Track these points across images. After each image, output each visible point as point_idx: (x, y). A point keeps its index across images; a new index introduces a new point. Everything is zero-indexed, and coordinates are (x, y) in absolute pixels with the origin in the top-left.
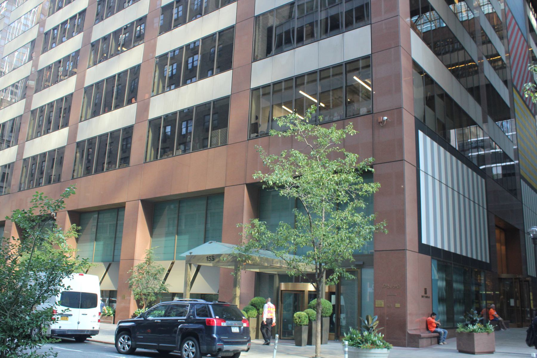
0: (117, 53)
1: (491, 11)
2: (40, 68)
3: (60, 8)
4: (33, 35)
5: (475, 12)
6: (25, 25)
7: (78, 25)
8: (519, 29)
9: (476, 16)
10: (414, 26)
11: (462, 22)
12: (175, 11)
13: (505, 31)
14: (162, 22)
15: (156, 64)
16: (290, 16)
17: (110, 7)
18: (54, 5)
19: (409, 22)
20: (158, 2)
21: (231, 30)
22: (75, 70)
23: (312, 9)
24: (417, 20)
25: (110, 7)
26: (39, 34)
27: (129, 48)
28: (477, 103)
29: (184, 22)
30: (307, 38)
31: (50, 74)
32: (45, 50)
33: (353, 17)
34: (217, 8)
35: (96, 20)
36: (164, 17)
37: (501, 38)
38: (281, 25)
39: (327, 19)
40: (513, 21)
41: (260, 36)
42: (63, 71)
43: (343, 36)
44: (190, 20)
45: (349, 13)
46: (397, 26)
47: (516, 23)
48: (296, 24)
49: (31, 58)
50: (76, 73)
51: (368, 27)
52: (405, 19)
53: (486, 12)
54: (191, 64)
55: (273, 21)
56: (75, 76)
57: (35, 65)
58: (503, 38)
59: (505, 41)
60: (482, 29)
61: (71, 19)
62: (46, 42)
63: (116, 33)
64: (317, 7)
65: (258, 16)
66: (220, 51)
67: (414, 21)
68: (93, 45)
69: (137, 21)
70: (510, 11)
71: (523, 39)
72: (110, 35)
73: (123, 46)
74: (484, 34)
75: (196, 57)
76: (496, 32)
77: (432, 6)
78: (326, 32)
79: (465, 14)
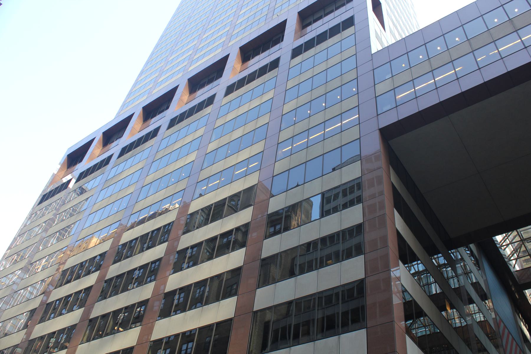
0: (113, 332)
1: (482, 319)
2: (32, 337)
3: (68, 282)
4: (35, 304)
5: (468, 319)
6: (31, 293)
7: (81, 300)
8: (513, 339)
9: (469, 322)
10: (408, 331)
11: (456, 328)
12: (177, 297)
13: (500, 339)
14: (162, 306)
15: (150, 347)
16: (288, 314)
17: (116, 286)
18: (64, 278)
19: (404, 325)
20: (162, 287)
21: (229, 322)
22: (68, 344)
23: (309, 307)
24: (411, 323)
25: (116, 286)
26: (42, 303)
27: (125, 329)
28: (294, 31)
29: (184, 310)
30: (303, 335)
31: (41, 344)
32: (42, 320)
33: (348, 320)
34: (218, 300)
35: (100, 296)
36: (165, 302)
37: (497, 347)
38: (277, 321)
39: (323, 318)
40: (506, 331)
41: (257, 330)
42: (54, 343)
43: (339, 338)
44: (190, 309)
45: (345, 314)
46: (392, 329)
47: (509, 333)
48: (293, 321)
49: (26, 326)
50: (66, 347)
51: (363, 332)
52: (401, 324)
53: (478, 320)
54: (184, 351)
55: (270, 316)
56: (66, 350)
57: (29, 334)
58: (498, 346)
59: (501, 350)
60: (476, 337)
61: (76, 293)
62: (46, 312)
63: (116, 313)
64: (314, 306)
65: (257, 312)
66: (215, 341)
67: (409, 325)
68: (91, 321)
69: (138, 303)
70: (501, 320)
71: (518, 349)
72: (109, 313)
73: (121, 325)
74: (479, 342)
75: (190, 345)
76: (490, 340)
77: (425, 313)
78: (322, 331)
79: (457, 321)
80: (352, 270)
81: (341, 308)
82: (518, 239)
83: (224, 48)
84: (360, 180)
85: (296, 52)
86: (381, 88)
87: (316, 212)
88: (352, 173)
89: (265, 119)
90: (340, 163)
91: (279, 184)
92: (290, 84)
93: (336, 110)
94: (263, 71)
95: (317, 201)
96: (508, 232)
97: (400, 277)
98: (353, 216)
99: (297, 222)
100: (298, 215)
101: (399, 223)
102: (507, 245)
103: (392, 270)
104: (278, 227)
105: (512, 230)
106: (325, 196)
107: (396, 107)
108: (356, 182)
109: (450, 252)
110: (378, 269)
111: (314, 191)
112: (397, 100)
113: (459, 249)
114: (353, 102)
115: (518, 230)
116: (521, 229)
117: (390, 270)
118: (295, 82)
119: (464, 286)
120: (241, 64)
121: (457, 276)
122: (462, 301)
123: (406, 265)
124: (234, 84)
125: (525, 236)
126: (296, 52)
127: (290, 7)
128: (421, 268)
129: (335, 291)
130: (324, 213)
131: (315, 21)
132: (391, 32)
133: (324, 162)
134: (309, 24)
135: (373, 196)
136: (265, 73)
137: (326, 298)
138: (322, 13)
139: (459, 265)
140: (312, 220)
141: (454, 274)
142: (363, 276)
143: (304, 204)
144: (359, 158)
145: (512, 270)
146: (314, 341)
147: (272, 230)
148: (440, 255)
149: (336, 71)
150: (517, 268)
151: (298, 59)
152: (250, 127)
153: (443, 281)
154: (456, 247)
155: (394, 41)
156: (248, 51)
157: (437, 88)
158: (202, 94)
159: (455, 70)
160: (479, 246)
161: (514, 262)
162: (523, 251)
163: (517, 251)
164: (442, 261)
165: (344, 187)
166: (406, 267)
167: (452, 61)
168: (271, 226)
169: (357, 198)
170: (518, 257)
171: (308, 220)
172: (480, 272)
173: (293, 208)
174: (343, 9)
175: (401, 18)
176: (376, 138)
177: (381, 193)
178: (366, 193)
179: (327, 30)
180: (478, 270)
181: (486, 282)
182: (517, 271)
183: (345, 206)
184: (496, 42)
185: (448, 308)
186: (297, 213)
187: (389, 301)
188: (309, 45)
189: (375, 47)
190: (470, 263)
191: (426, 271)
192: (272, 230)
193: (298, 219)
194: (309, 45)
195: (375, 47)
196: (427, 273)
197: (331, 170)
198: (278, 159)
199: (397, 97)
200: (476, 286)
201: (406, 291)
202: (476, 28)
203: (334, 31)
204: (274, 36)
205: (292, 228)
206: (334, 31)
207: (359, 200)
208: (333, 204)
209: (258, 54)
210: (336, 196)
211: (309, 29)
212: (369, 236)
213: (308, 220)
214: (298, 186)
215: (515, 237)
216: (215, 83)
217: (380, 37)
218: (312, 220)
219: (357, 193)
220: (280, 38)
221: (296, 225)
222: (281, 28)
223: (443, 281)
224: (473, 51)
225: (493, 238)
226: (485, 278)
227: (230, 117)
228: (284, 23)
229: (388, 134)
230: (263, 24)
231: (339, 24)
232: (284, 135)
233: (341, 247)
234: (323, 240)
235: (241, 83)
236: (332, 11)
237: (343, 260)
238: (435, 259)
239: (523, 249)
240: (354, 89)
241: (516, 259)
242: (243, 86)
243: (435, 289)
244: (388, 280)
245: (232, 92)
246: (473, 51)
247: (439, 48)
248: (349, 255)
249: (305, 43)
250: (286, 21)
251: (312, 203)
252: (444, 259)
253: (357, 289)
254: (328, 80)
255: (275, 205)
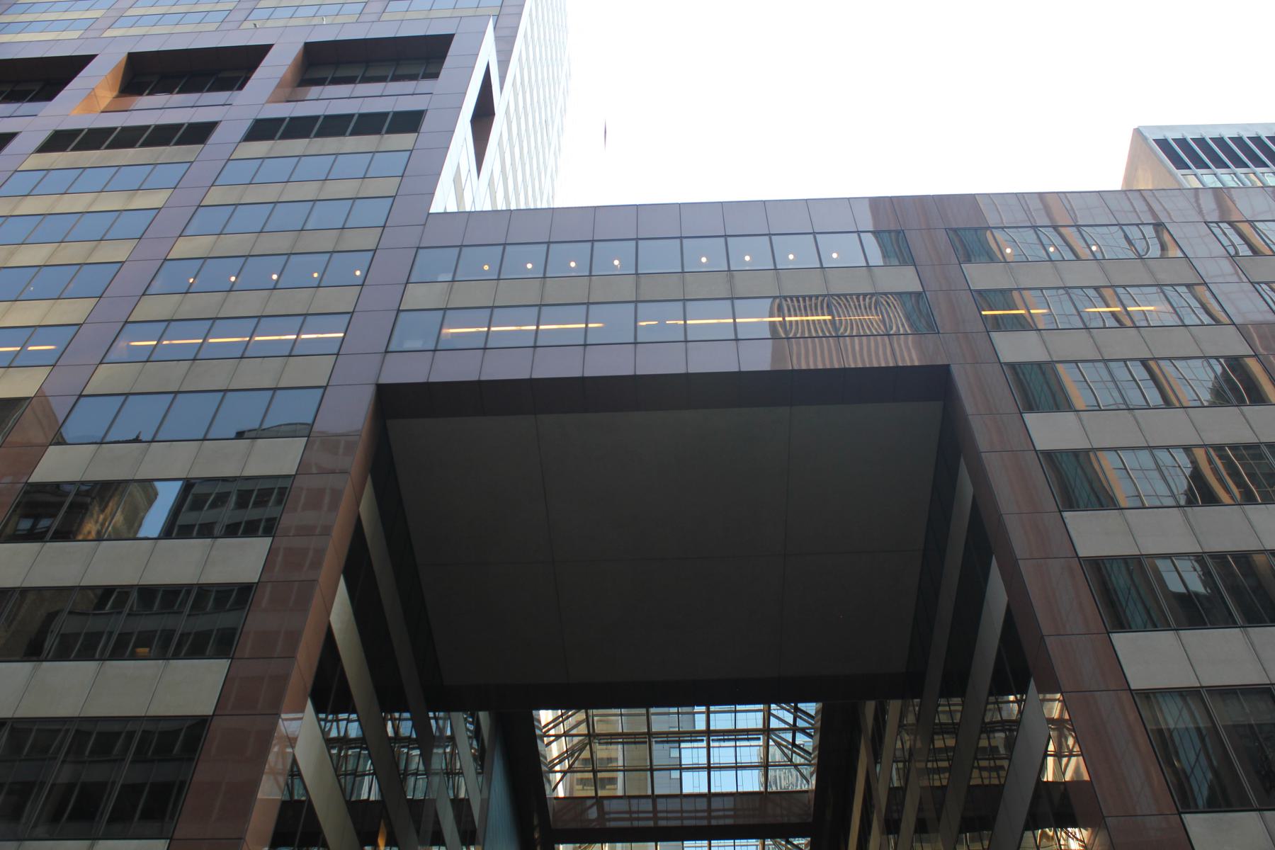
39: (70, 787)
43: (92, 846)
80: (186, 687)
81: (124, 774)
82: (583, 729)
83: (91, 34)
84: (287, 484)
85: (262, 130)
86: (417, 296)
87: (154, 521)
88: (277, 459)
89: (118, 251)
90: (256, 426)
91: (80, 424)
92: (215, 196)
93: (297, 301)
94: (162, 135)
95: (168, 494)
96: (568, 708)
97: (296, 739)
98: (241, 560)
99: (98, 526)
100: (108, 510)
101: (340, 613)
102: (558, 737)
103: (283, 716)
104: (44, 523)
105: (578, 707)
106: (194, 490)
107: (435, 351)
108: (280, 484)
109: (431, 714)
110: (252, 705)
111: (169, 468)
112: (442, 337)
113: (453, 714)
114: (343, 300)
115: (590, 712)
116: (595, 711)
117: (278, 715)
118: (231, 196)
119: (434, 801)
120: (115, 94)
121: (428, 772)
122: (418, 832)
123: (322, 716)
124: (76, 132)
125: (599, 728)
126: (262, 130)
127: (293, 22)
128: (354, 731)
129: (129, 727)
130: (173, 529)
131: (336, 81)
132: (491, 183)
133: (72, 416)
134: (320, 82)
135: (305, 531)
136: (132, 145)
137: (96, 737)
138: (359, 72)
139: (441, 751)
140: (140, 535)
141: (421, 767)
142: (208, 710)
143: (134, 488)
144: (305, 430)
145: (548, 792)
146: (20, 839)
147: (25, 524)
148: (406, 715)
149: (335, 215)
150: (561, 792)
151: (260, 148)
152: (72, 253)
153: (393, 776)
154: (448, 708)
155: (488, 207)
156: (145, 73)
157: (535, 347)
158: (156, 109)
159: (159, 340)
160: (500, 723)
161: (559, 776)
162: (585, 760)
163: (572, 755)
164: (406, 729)
165: (267, 485)
166: (319, 720)
167: (588, 304)
168: (26, 516)
169: (268, 520)
170: (571, 770)
171: (130, 532)
172: (480, 779)
173: (104, 491)
174: (344, 90)
175: (523, 165)
176: (365, 398)
177: (326, 531)
178: (289, 520)
179: (353, 115)
180: (478, 774)
181: (485, 805)
182: (557, 798)
183: (232, 531)
184: (688, 303)
185: (381, 842)
186: (106, 507)
187: (254, 785)
188: (299, 128)
189: (444, 201)
190: (466, 750)
191: (360, 742)
192: (25, 524)
193: (105, 520)
194: (299, 128)
195: (444, 201)
196: (362, 749)
197: (233, 435)
198: (112, 356)
199: (445, 331)
200: (461, 807)
201: (300, 775)
202: (660, 258)
203: (370, 124)
204: (226, 67)
205: (80, 537)
206: (370, 124)
207: (269, 528)
208: (205, 515)
209: (169, 91)
210: (221, 499)
211: (314, 91)
212: (257, 620)
213: (130, 532)
214: (137, 440)
215: (578, 724)
216: (27, 107)
217: (464, 184)
218: (140, 535)
219: (270, 510)
220: (239, 78)
221: (93, 535)
222: (250, 58)
223: (393, 776)
224: (636, 302)
225: (534, 712)
226: (485, 795)
227: (30, 206)
228: (263, 50)
229: (393, 402)
230: (213, 27)
231: (386, 114)
232: (150, 308)
233: (182, 623)
234: (147, 593)
235: (94, 139)
236: (413, 77)
237: (176, 656)
238: (393, 720)
239: (586, 754)
240: (358, 273)
241: (564, 773)
242: (98, 148)
243: (369, 790)
244: (266, 738)
245: (63, 149)
246: (636, 302)
247: (704, 260)
248: (197, 648)
249: (292, 119)
250: (269, 47)
251: (156, 495)
252: (413, 726)
253: (180, 739)
254: (308, 226)
255: (57, 466)
